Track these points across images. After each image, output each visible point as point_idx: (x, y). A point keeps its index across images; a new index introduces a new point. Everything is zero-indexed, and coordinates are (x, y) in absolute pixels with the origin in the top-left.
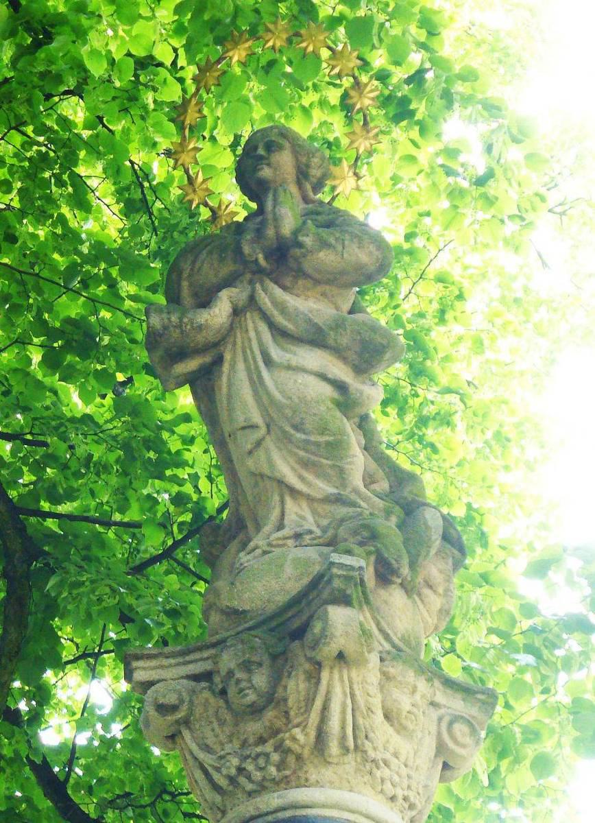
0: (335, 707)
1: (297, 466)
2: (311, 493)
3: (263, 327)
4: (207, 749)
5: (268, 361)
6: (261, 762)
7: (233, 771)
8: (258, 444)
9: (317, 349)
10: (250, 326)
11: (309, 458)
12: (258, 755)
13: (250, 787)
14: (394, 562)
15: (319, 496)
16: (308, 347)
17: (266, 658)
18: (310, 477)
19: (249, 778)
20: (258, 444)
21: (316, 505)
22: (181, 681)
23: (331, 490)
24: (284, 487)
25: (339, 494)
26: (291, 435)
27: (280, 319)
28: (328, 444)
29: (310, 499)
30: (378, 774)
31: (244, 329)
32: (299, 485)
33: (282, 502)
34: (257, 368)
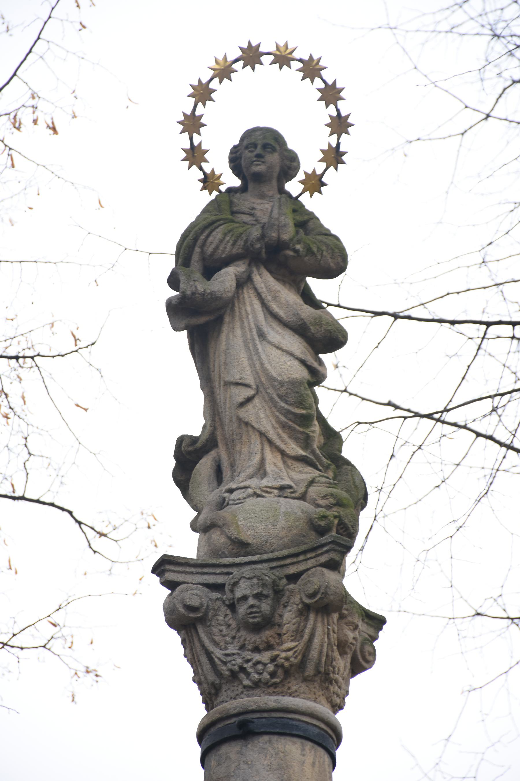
0: (317, 641)
1: (276, 425)
2: (286, 450)
3: (257, 305)
4: (216, 644)
5: (262, 335)
6: (260, 667)
7: (236, 668)
8: (249, 400)
9: (297, 336)
10: (246, 296)
11: (287, 423)
12: (258, 662)
13: (246, 682)
14: (351, 528)
15: (292, 454)
16: (291, 332)
17: (271, 592)
18: (285, 436)
19: (248, 674)
20: (249, 400)
21: (286, 459)
22: (199, 586)
23: (302, 452)
24: (265, 439)
25: (306, 456)
26: (276, 402)
27: (275, 307)
28: (302, 416)
29: (283, 453)
30: (331, 688)
31: (242, 300)
32: (278, 442)
33: (262, 449)
34: (253, 340)
